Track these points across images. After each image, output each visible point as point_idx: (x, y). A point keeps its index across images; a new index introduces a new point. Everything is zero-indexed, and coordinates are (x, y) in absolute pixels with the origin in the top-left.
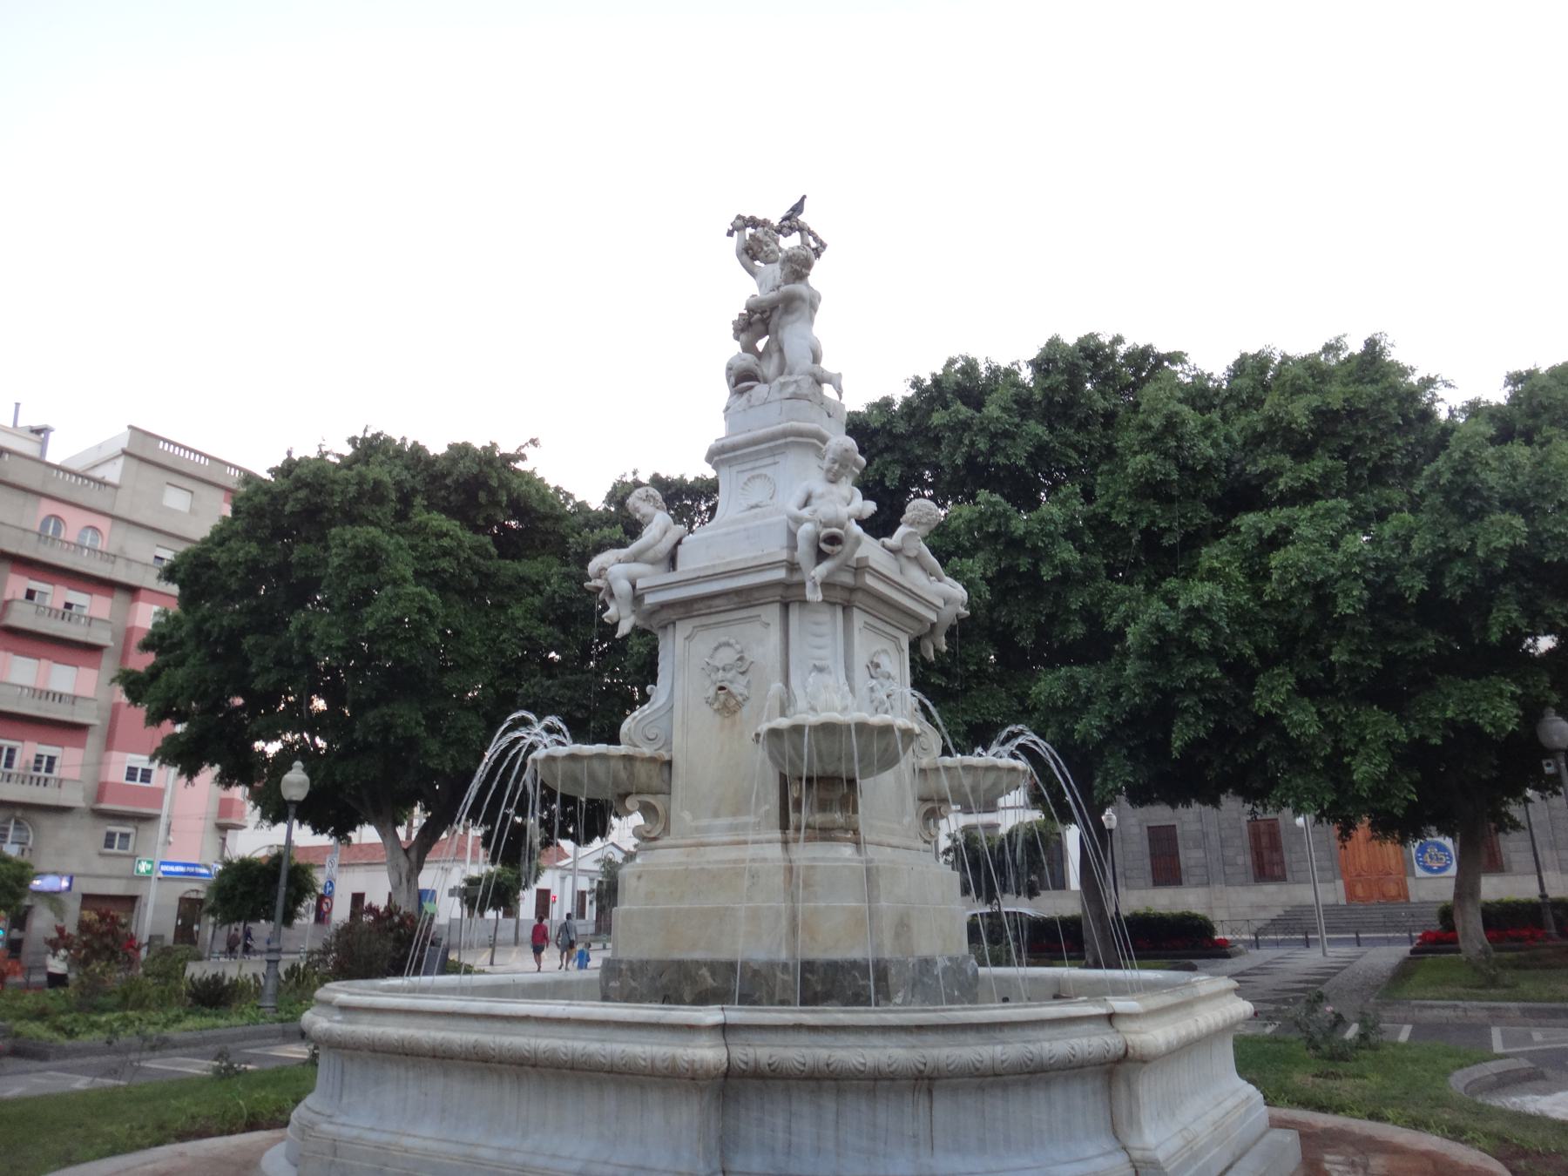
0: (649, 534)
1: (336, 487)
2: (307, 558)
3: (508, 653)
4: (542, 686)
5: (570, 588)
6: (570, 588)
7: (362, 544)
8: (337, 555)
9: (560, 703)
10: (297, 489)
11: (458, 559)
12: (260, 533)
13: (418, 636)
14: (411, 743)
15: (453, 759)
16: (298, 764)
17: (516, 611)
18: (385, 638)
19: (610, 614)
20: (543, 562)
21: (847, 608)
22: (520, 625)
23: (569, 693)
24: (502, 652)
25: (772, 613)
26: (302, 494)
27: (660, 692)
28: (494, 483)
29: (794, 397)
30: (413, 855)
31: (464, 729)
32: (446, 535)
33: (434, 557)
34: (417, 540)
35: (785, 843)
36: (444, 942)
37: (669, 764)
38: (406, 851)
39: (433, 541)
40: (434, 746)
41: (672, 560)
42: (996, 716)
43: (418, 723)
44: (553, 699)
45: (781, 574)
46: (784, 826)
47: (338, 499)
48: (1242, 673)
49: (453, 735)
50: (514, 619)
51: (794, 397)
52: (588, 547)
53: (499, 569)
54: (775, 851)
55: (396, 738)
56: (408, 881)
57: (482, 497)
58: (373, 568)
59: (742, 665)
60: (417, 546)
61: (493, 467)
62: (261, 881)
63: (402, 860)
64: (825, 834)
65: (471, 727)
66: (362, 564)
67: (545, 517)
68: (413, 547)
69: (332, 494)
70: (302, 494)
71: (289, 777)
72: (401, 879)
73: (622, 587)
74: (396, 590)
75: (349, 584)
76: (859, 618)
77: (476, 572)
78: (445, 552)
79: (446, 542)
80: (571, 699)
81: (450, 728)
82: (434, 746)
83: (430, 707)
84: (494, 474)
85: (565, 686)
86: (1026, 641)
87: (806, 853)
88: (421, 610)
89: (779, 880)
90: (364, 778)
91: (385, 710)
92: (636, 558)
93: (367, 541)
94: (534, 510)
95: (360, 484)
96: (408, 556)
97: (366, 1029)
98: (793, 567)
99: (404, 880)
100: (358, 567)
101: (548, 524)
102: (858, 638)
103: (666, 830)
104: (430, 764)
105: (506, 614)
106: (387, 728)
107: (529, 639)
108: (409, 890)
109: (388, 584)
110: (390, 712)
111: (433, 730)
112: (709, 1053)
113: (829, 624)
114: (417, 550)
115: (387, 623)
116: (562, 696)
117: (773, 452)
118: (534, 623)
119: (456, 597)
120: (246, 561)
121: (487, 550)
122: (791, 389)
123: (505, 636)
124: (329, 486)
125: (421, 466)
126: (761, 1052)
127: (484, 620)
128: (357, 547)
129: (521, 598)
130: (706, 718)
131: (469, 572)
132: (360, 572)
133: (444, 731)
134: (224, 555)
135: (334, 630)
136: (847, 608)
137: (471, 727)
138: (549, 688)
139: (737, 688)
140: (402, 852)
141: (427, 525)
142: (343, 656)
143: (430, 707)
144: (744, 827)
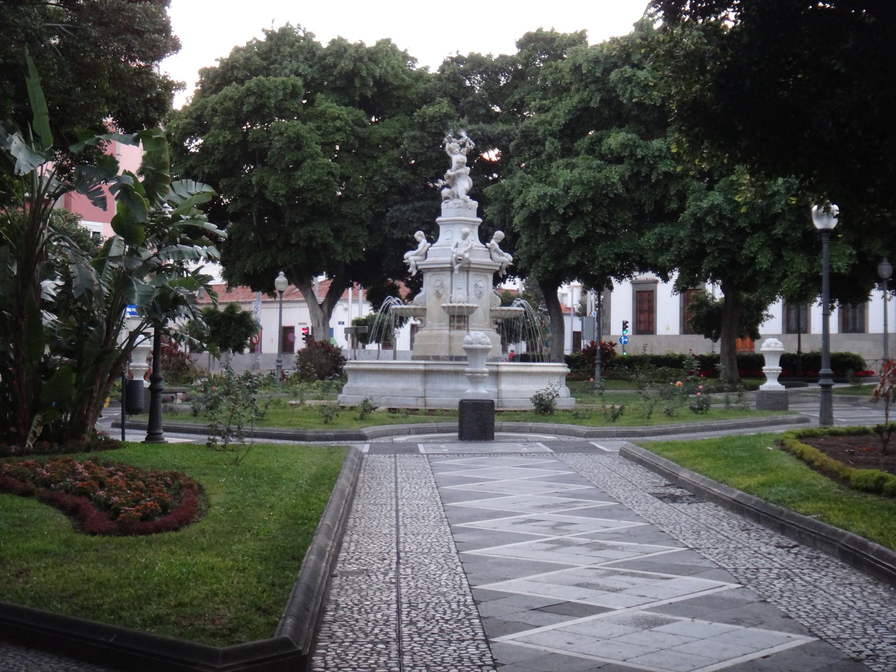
0: (420, 246)
1: (272, 94)
2: (257, 138)
3: (380, 189)
4: (401, 211)
5: (416, 147)
6: (416, 147)
7: (292, 135)
8: (278, 141)
9: (411, 222)
10: (248, 95)
11: (345, 132)
12: (229, 125)
13: (328, 188)
14: (325, 246)
15: (350, 255)
16: (282, 273)
17: (383, 161)
18: (309, 190)
19: (410, 270)
20: (397, 121)
21: (468, 272)
22: (386, 170)
23: (417, 215)
24: (376, 189)
25: (449, 273)
26: (252, 99)
27: (423, 289)
28: (364, 73)
29: (458, 208)
30: (325, 308)
31: (356, 237)
32: (338, 118)
33: (332, 133)
34: (320, 123)
35: (450, 330)
36: (208, 442)
37: (425, 309)
38: (321, 306)
39: (330, 124)
40: (339, 248)
41: (426, 255)
42: (631, 249)
43: (329, 235)
44: (408, 219)
45: (449, 265)
46: (450, 326)
47: (273, 101)
48: (742, 235)
49: (349, 240)
50: (381, 167)
51: (458, 208)
52: (425, 118)
53: (371, 133)
54: (447, 332)
55: (317, 244)
56: (324, 325)
57: (357, 83)
58: (299, 148)
59: (442, 286)
60: (321, 126)
61: (362, 62)
62: (223, 323)
63: (319, 311)
64: (459, 328)
65: (360, 235)
66: (293, 146)
67: (398, 88)
68: (318, 128)
69: (269, 98)
70: (252, 99)
71: (278, 280)
72: (319, 324)
73: (413, 263)
74: (314, 162)
75: (286, 159)
76: (471, 274)
77: (357, 137)
78: (338, 130)
79: (338, 123)
80: (419, 219)
81: (347, 237)
82: (339, 248)
83: (335, 224)
84: (364, 67)
85: (415, 210)
86: (649, 208)
87: (455, 333)
88: (329, 173)
89: (447, 339)
90: (295, 263)
91: (310, 228)
92: (416, 255)
93: (295, 133)
94: (391, 84)
95: (284, 89)
96: (316, 136)
97: (361, 367)
98: (451, 263)
99: (321, 324)
100: (290, 148)
101: (401, 93)
102: (470, 278)
103: (425, 326)
104: (338, 259)
105: (376, 162)
106: (311, 238)
107: (391, 179)
108: (324, 331)
109: (308, 158)
110: (312, 229)
111: (337, 238)
112: (421, 368)
113: (463, 276)
114: (321, 129)
115: (310, 182)
116: (413, 217)
117: (453, 224)
118: (393, 168)
119: (346, 155)
120: (224, 142)
121: (362, 121)
122: (458, 205)
123: (376, 178)
124: (267, 93)
125: (316, 59)
126: (430, 368)
127: (364, 167)
128: (289, 137)
129: (386, 151)
130: (434, 297)
131: (352, 138)
132: (292, 151)
133: (344, 239)
134: (210, 139)
135: (279, 184)
136: (468, 272)
137: (360, 235)
138: (406, 211)
139: (441, 292)
140: (318, 307)
141: (326, 112)
142: (286, 200)
143: (335, 224)
144: (441, 326)
